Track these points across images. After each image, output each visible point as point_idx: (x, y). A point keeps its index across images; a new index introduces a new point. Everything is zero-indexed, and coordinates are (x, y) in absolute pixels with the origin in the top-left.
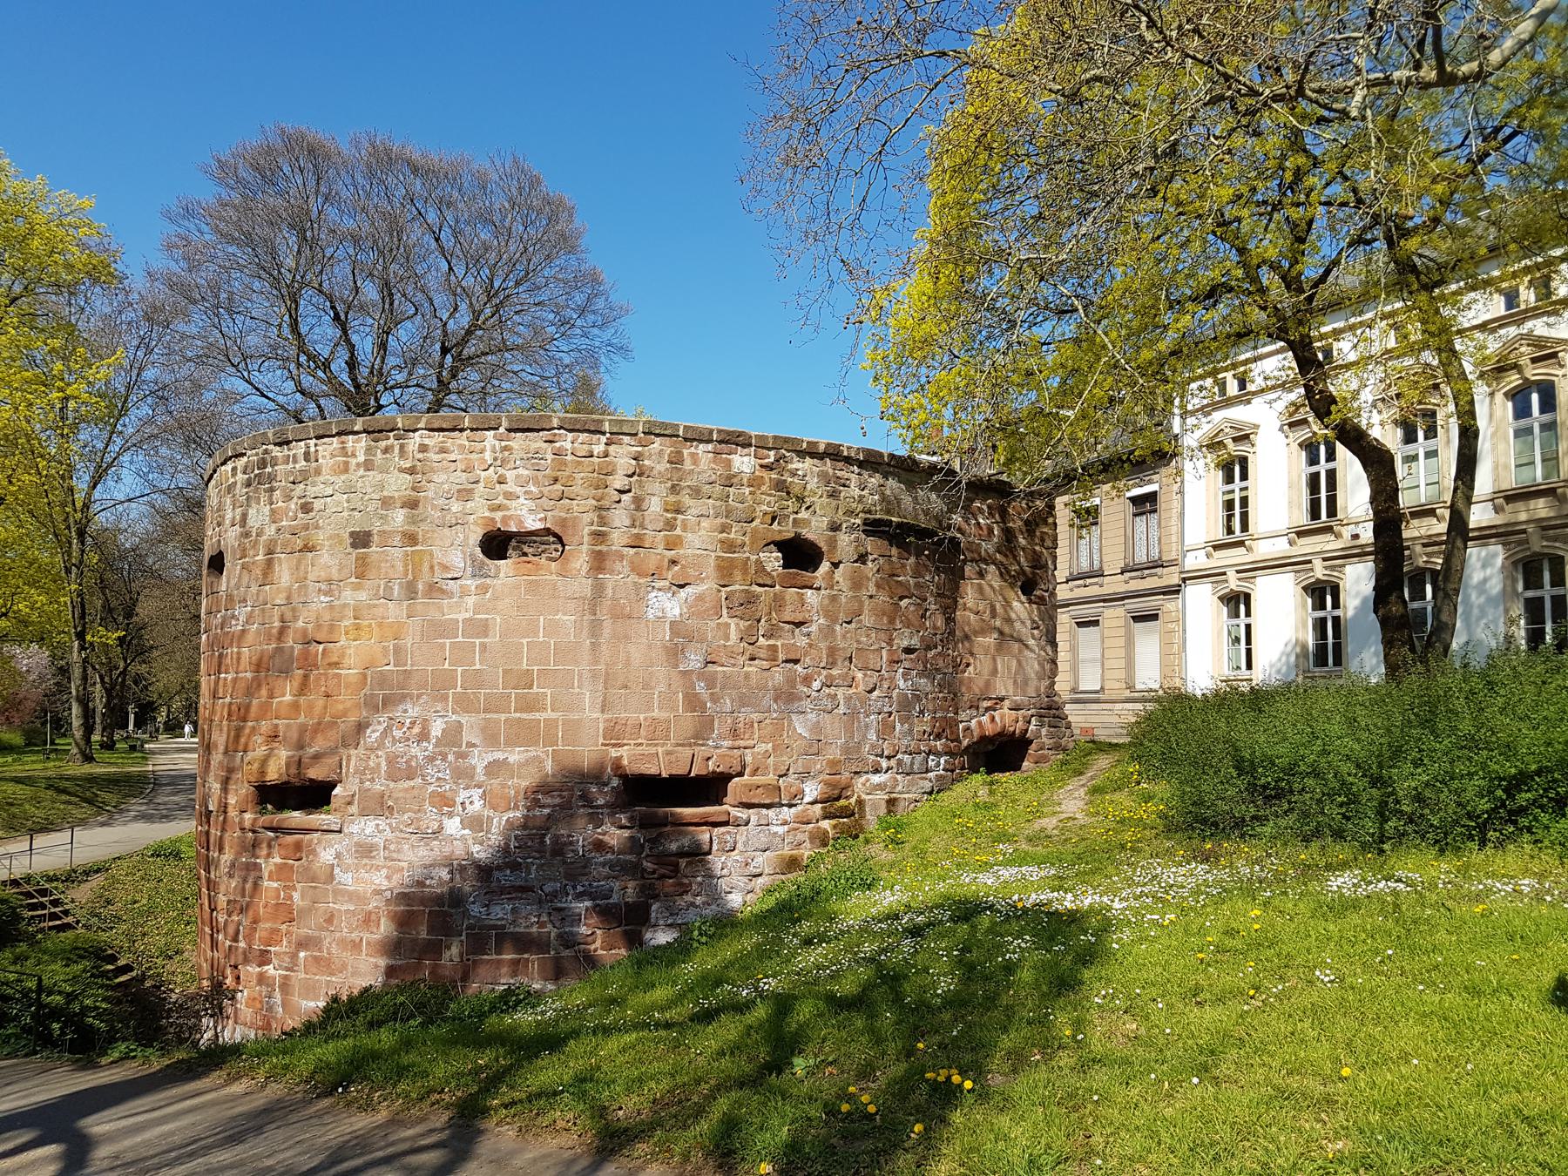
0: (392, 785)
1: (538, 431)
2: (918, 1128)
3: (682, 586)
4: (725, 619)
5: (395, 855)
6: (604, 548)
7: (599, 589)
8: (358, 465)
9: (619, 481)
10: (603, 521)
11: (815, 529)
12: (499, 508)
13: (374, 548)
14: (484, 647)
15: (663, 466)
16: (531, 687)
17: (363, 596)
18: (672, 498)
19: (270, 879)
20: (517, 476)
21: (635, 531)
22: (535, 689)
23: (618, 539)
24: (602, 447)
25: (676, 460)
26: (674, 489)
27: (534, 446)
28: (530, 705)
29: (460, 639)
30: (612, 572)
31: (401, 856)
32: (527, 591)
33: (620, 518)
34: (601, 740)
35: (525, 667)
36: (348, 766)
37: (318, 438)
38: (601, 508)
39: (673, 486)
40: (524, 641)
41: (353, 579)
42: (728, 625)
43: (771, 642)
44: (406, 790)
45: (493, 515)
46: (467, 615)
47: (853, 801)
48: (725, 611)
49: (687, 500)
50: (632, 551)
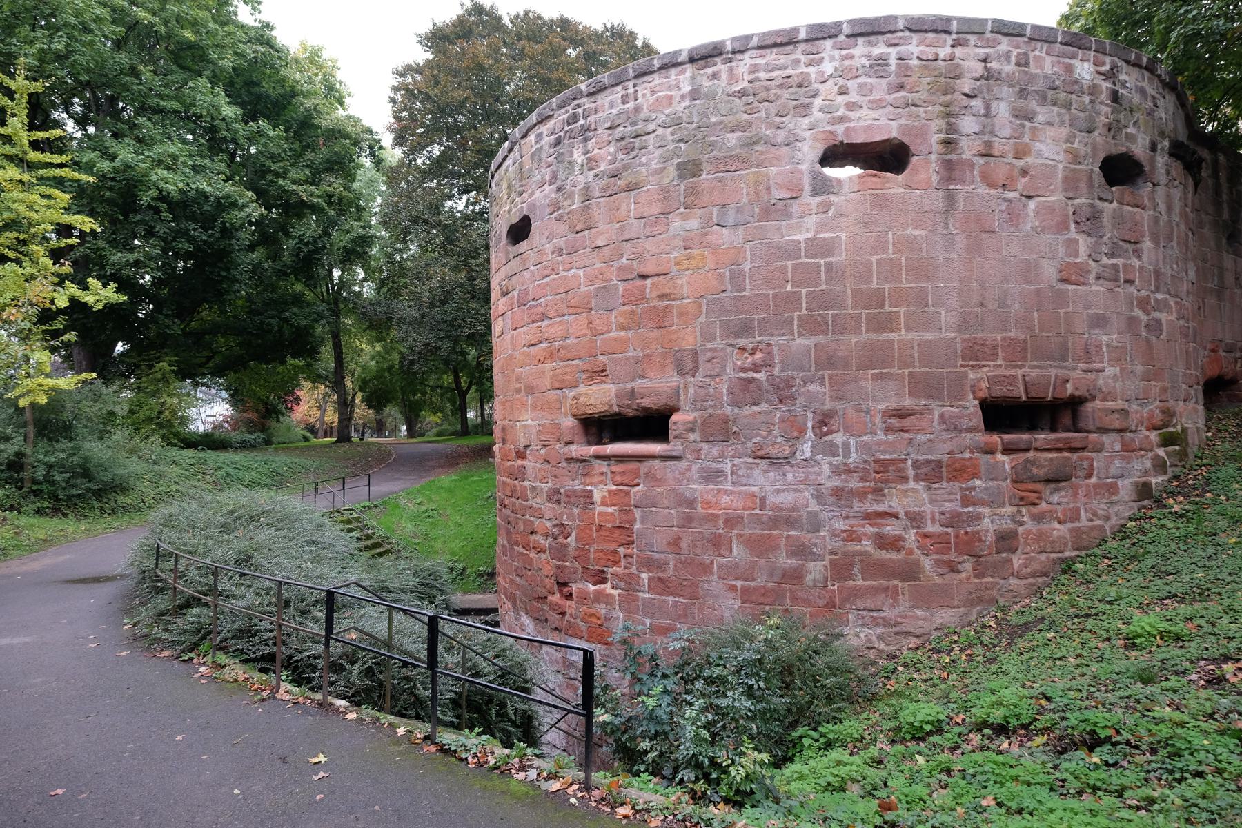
0: (737, 411)
1: (883, 33)
2: (322, 758)
3: (1029, 197)
4: (1073, 233)
5: (744, 480)
6: (953, 157)
7: (950, 199)
8: (683, 97)
9: (966, 85)
10: (951, 128)
11: (1139, 149)
12: (842, 120)
13: (704, 176)
14: (829, 268)
15: (1009, 68)
16: (882, 306)
17: (694, 223)
18: (1021, 103)
19: (604, 504)
20: (860, 85)
21: (986, 138)
22: (887, 309)
23: (968, 148)
24: (948, 50)
25: (1023, 62)
26: (1023, 93)
27: (877, 51)
28: (884, 324)
29: (803, 260)
30: (963, 182)
31: (751, 481)
32: (874, 206)
33: (968, 124)
34: (960, 362)
35: (874, 285)
36: (686, 395)
37: (636, 77)
38: (949, 115)
39: (1022, 90)
40: (873, 259)
41: (682, 210)
42: (1077, 241)
43: (1114, 261)
44: (752, 416)
45: (833, 128)
46: (809, 235)
47: (1179, 428)
48: (1073, 226)
49: (1033, 105)
50: (981, 161)
